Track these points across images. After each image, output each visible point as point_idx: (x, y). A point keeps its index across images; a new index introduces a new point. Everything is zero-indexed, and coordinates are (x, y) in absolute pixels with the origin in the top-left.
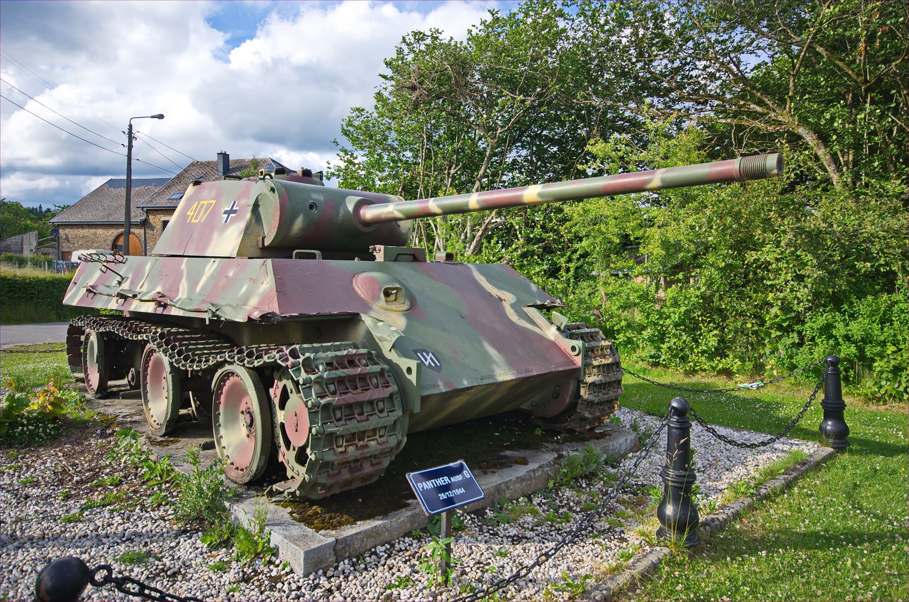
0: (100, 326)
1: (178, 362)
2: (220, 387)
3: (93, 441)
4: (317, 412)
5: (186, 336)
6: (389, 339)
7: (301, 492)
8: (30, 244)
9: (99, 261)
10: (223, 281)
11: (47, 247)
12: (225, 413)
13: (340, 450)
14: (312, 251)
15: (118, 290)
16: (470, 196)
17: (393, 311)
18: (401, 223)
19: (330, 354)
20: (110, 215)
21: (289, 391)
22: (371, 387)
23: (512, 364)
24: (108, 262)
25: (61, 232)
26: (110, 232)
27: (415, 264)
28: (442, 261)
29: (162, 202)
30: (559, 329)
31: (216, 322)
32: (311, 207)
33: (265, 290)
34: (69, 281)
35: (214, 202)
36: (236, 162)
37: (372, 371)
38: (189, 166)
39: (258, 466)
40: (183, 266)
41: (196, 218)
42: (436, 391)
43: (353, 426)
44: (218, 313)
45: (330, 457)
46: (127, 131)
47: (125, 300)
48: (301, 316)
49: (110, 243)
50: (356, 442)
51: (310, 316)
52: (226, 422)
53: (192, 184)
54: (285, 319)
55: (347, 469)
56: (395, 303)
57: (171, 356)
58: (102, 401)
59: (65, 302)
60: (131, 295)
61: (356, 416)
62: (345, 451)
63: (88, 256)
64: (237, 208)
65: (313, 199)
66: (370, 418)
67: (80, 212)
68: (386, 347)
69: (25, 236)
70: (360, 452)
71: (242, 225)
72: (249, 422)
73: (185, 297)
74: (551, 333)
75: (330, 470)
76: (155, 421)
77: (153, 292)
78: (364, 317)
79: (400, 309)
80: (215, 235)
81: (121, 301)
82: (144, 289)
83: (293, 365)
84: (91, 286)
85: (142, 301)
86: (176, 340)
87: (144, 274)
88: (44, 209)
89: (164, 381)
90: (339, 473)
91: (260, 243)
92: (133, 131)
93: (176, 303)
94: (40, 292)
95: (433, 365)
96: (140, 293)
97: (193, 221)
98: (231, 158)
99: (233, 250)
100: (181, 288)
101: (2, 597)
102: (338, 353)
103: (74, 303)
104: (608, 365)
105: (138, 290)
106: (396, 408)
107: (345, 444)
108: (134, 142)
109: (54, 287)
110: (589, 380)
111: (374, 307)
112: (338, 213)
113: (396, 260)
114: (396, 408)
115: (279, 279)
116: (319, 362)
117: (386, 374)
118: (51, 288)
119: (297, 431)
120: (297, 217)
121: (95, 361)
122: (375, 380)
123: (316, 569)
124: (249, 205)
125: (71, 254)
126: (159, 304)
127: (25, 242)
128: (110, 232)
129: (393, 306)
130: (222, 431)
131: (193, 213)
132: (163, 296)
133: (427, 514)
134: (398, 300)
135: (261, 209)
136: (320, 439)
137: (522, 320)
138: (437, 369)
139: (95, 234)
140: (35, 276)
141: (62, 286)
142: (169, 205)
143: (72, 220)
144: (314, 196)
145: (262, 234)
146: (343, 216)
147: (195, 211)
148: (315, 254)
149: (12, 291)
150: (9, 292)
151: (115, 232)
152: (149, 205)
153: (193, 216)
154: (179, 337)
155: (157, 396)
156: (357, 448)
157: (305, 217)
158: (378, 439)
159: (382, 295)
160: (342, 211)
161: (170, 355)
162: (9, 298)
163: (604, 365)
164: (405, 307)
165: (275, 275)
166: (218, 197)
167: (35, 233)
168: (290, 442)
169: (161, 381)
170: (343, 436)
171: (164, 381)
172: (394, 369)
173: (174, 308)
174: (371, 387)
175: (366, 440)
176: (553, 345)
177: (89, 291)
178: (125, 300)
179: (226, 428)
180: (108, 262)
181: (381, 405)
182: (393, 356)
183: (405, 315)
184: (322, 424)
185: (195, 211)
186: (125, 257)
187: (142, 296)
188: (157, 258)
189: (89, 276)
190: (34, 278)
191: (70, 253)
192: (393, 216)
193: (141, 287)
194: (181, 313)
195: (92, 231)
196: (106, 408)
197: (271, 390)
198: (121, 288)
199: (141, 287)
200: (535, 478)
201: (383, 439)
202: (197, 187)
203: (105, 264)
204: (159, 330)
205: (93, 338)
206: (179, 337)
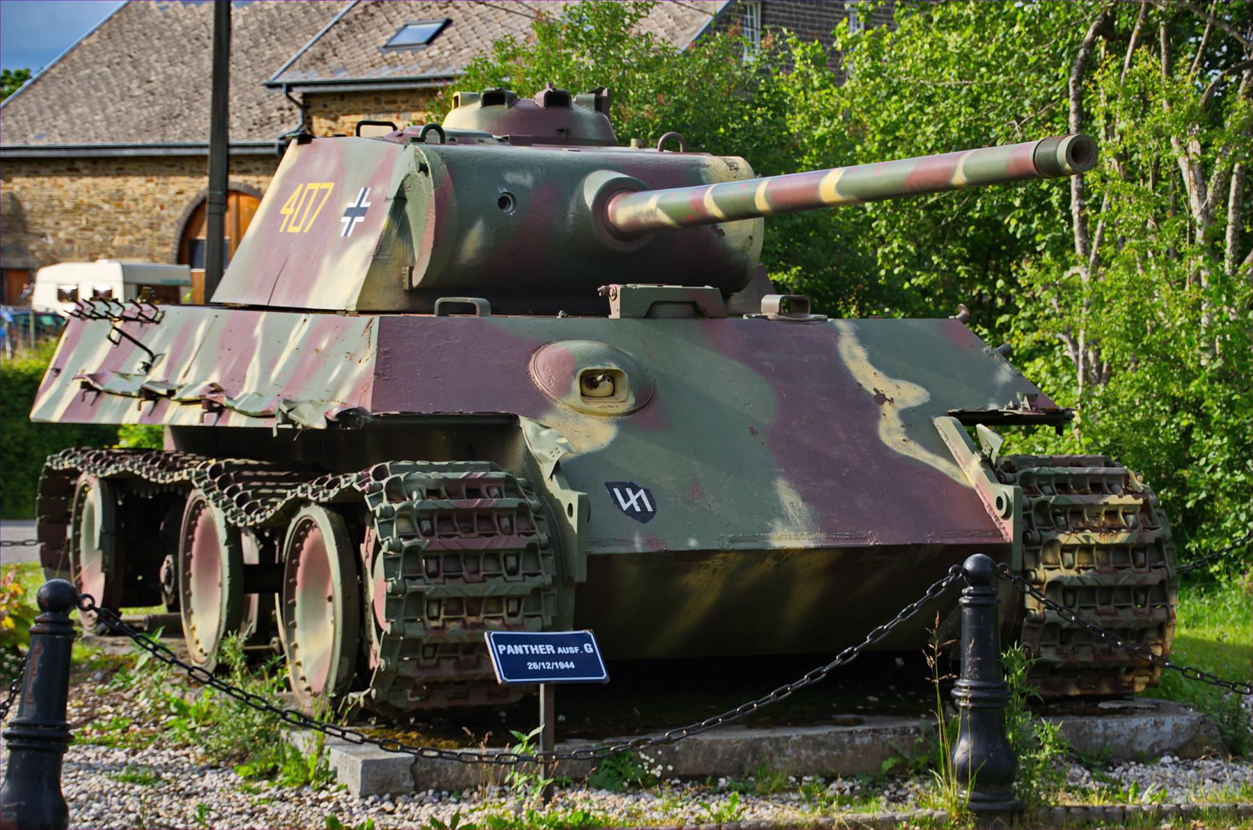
0: (108, 466)
1: (234, 515)
2: (295, 553)
3: (86, 687)
5: (259, 473)
6: (550, 457)
7: (377, 693)
9: (108, 316)
10: (312, 356)
13: (435, 624)
17: (594, 413)
18: (731, 228)
19: (434, 475)
20: (170, 117)
22: (498, 531)
23: (821, 523)
26: (173, 189)
27: (695, 324)
28: (771, 315)
30: (986, 461)
32: (503, 202)
34: (40, 373)
37: (500, 506)
39: (338, 678)
40: (258, 331)
41: (296, 224)
43: (455, 588)
45: (415, 631)
47: (156, 402)
48: (404, 415)
49: (171, 232)
50: (465, 615)
51: (421, 416)
52: (304, 617)
53: (294, 142)
54: (379, 421)
55: (452, 662)
56: (611, 399)
57: (226, 506)
58: (110, 639)
59: (37, 413)
60: (163, 391)
61: (465, 573)
62: (444, 627)
63: (86, 306)
66: (489, 580)
67: (65, 107)
68: (547, 469)
70: (469, 631)
71: (370, 243)
73: (253, 390)
74: (971, 472)
75: (420, 656)
76: (201, 651)
77: (205, 384)
79: (610, 411)
80: (326, 261)
81: (147, 405)
82: (190, 379)
83: (372, 489)
86: (239, 478)
87: (191, 348)
90: (437, 666)
91: (406, 281)
93: (236, 402)
95: (638, 509)
96: (180, 387)
97: (291, 229)
99: (352, 296)
100: (249, 374)
101: (8, 623)
102: (450, 475)
103: (56, 417)
105: (179, 380)
106: (542, 571)
107: (442, 616)
110: (1044, 574)
111: (559, 406)
113: (650, 315)
114: (542, 571)
115: (385, 353)
116: (413, 486)
117: (532, 515)
120: (471, 225)
121: (96, 544)
122: (506, 522)
123: (381, 791)
124: (387, 199)
125: (31, 280)
126: (211, 406)
129: (595, 406)
131: (291, 211)
133: (500, 681)
134: (617, 395)
135: (409, 208)
136: (400, 601)
137: (911, 444)
138: (644, 516)
139: (117, 198)
142: (385, 73)
144: (510, 177)
145: (409, 261)
146: (574, 219)
147: (296, 207)
152: (314, 76)
153: (291, 216)
154: (246, 473)
156: (465, 625)
158: (506, 617)
159: (576, 385)
160: (572, 208)
161: (224, 504)
163: (1099, 547)
164: (623, 408)
170: (439, 602)
172: (551, 504)
174: (498, 531)
175: (482, 615)
176: (971, 496)
177: (86, 386)
178: (156, 402)
179: (304, 629)
180: (126, 319)
181: (512, 562)
183: (618, 423)
184: (404, 578)
185: (296, 207)
187: (185, 392)
193: (185, 376)
195: (108, 184)
196: (116, 648)
198: (149, 378)
199: (185, 376)
200: (853, 748)
201: (514, 620)
202: (305, 147)
203: (119, 325)
204: (213, 462)
205: (94, 497)
206: (246, 473)
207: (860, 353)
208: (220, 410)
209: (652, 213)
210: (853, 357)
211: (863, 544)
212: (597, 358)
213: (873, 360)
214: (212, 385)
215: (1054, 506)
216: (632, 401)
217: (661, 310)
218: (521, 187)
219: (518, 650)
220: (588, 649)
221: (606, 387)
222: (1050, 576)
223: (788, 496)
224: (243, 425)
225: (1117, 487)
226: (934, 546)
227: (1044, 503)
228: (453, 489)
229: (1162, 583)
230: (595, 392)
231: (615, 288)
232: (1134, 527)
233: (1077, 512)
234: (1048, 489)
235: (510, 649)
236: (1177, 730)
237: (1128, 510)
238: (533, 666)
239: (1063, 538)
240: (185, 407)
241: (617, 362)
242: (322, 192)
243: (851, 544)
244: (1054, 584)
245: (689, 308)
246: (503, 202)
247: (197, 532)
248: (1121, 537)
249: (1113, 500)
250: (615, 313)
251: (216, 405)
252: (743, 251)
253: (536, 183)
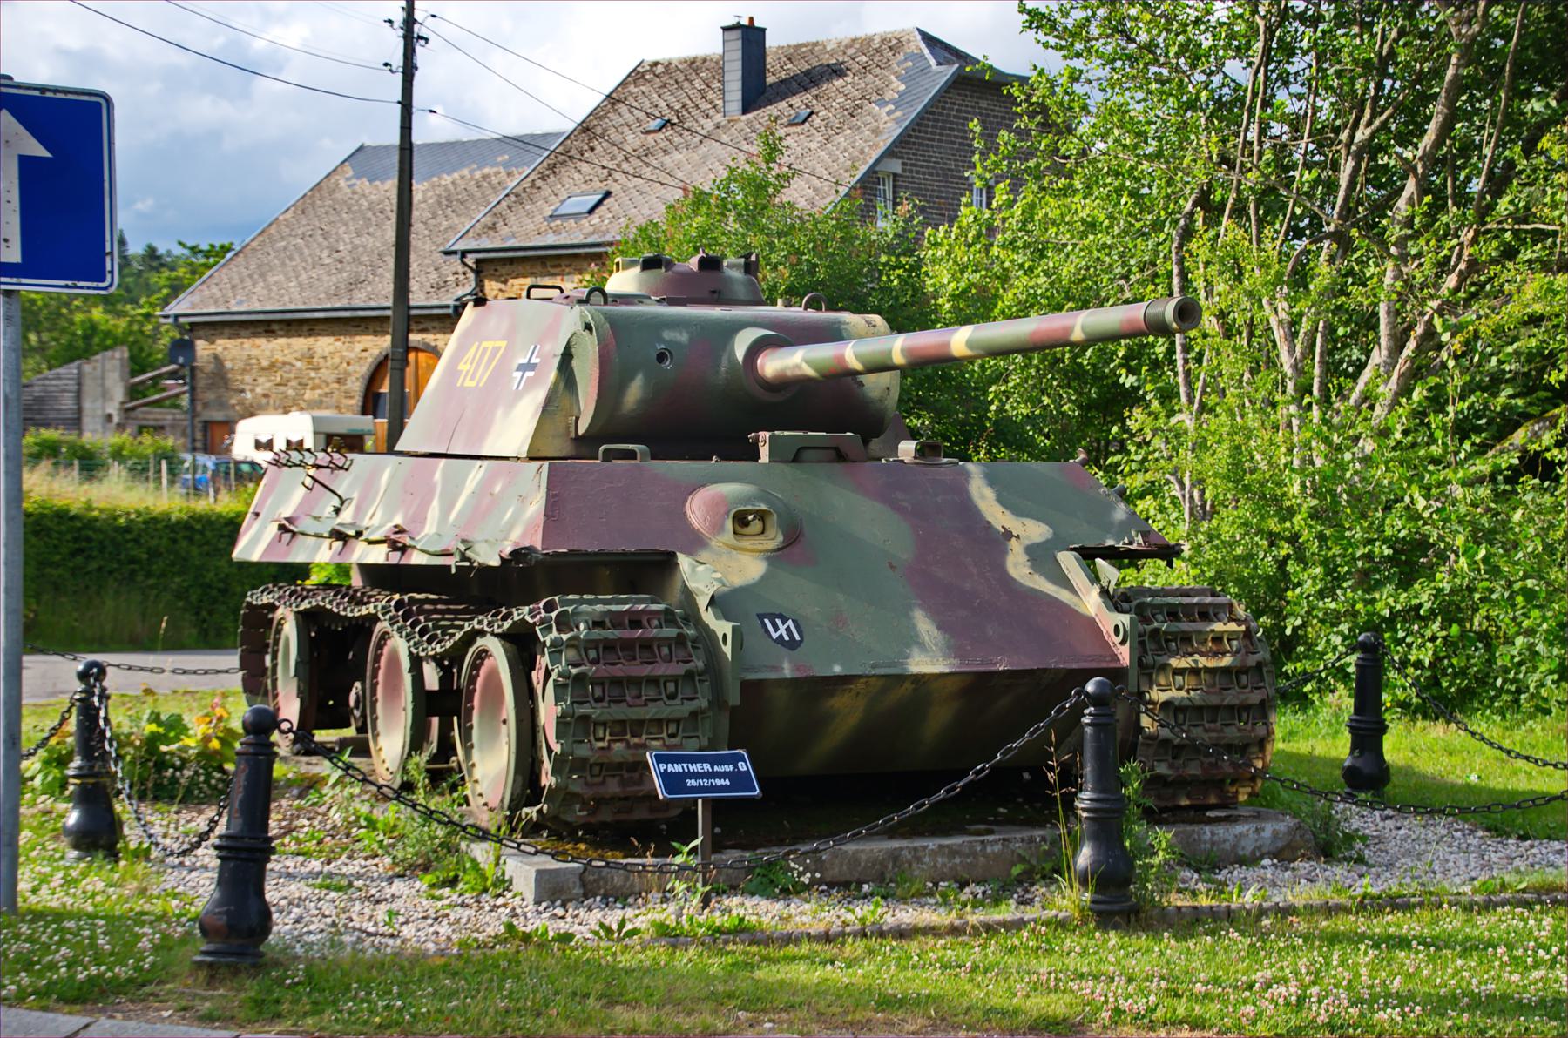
1: (416, 645)
2: (472, 680)
4: (565, 686)
8: (105, 395)
9: (302, 464)
11: (157, 403)
12: (481, 715)
14: (630, 447)
15: (336, 523)
18: (864, 379)
19: (599, 608)
20: (356, 283)
24: (318, 467)
25: (201, 346)
26: (358, 347)
27: (838, 467)
28: (908, 459)
30: (1104, 592)
32: (661, 357)
35: (503, 344)
36: (794, 52)
38: (623, 84)
40: (438, 476)
41: (472, 378)
42: (773, 676)
43: (619, 712)
48: (572, 553)
49: (356, 386)
51: (586, 554)
53: (470, 304)
57: (409, 637)
59: (238, 554)
60: (352, 533)
62: (609, 748)
69: (87, 368)
71: (540, 395)
73: (434, 530)
74: (1090, 602)
75: (587, 774)
78: (684, 561)
79: (760, 547)
80: (499, 413)
81: (338, 544)
83: (542, 621)
84: (287, 519)
85: (371, 543)
86: (420, 612)
90: (603, 783)
92: (418, 15)
94: (154, 554)
97: (469, 383)
98: (771, 42)
102: (614, 608)
104: (1225, 671)
105: (366, 523)
109: (191, 540)
110: (1157, 695)
111: (713, 543)
113: (796, 459)
118: (184, 544)
120: (632, 378)
121: (292, 672)
122: (665, 651)
125: (232, 432)
126: (395, 546)
127: (90, 387)
128: (358, 347)
129: (746, 543)
132: (402, 531)
135: (574, 363)
137: (1037, 577)
139: (309, 357)
140: (141, 506)
141: (231, 528)
142: (551, 240)
144: (668, 335)
149: (81, 551)
150: (74, 554)
154: (427, 607)
156: (628, 746)
157: (647, 379)
159: (729, 524)
160: (725, 362)
162: (74, 571)
164: (772, 545)
165: (548, 489)
166: (510, 336)
167: (122, 353)
170: (604, 724)
176: (1091, 623)
177: (282, 528)
179: (481, 749)
180: (318, 467)
181: (671, 687)
182: (709, 617)
183: (768, 559)
186: (350, 456)
189: (285, 497)
190: (139, 514)
191: (229, 427)
195: (300, 343)
198: (339, 520)
201: (674, 741)
202: (480, 309)
205: (290, 630)
206: (427, 607)
207: (989, 493)
209: (798, 366)
210: (983, 497)
211: (993, 668)
212: (749, 500)
213: (1001, 500)
215: (1166, 633)
216: (780, 538)
217: (807, 454)
218: (679, 344)
219: (677, 768)
220: (742, 767)
221: (756, 526)
222: (1162, 697)
223: (925, 626)
225: (1221, 615)
226: (1058, 670)
227: (1157, 630)
228: (616, 620)
229: (1263, 702)
230: (747, 530)
231: (764, 435)
232: (1238, 651)
233: (1186, 638)
234: (1160, 617)
235: (670, 768)
236: (1275, 835)
237: (1232, 636)
238: (691, 783)
239: (1175, 662)
241: (767, 502)
242: (496, 350)
243: (982, 669)
244: (1167, 705)
245: (832, 453)
246: (661, 357)
248: (1226, 661)
249: (1218, 627)
250: (764, 458)
252: (881, 400)
253: (691, 339)
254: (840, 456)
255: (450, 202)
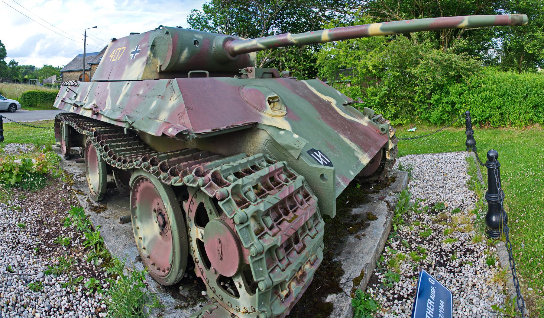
12: (140, 208)
16: (287, 35)
20: (79, 67)
21: (208, 212)
24: (71, 85)
29: (96, 61)
31: (132, 132)
32: (195, 43)
33: (173, 106)
35: (125, 48)
40: (108, 87)
41: (115, 59)
44: (134, 125)
46: (84, 34)
60: (79, 105)
64: (131, 55)
65: (196, 38)
71: (144, 59)
72: (162, 223)
73: (110, 108)
80: (127, 67)
81: (75, 108)
82: (87, 102)
87: (87, 93)
88: (59, 67)
89: (97, 162)
96: (84, 104)
97: (113, 60)
99: (139, 75)
100: (107, 102)
105: (84, 102)
106: (320, 220)
108: (87, 38)
112: (212, 47)
116: (246, 189)
119: (221, 259)
120: (184, 50)
126: (94, 113)
130: (138, 224)
139: (74, 75)
143: (67, 70)
144: (196, 36)
146: (215, 49)
148: (205, 73)
151: (80, 74)
155: (94, 171)
157: (189, 50)
159: (267, 103)
164: (285, 113)
167: (56, 75)
168: (210, 264)
169: (96, 162)
171: (97, 162)
173: (103, 116)
177: (62, 101)
179: (141, 221)
187: (85, 106)
188: (93, 83)
192: (257, 47)
194: (107, 121)
195: (73, 73)
197: (184, 203)
202: (114, 42)
203: (69, 87)
208: (98, 114)
214: (94, 105)
218: (200, 39)
224: (107, 122)
240: (85, 110)
242: (122, 50)
247: (90, 149)
251: (96, 112)
254: (273, 76)
255: (89, 59)
